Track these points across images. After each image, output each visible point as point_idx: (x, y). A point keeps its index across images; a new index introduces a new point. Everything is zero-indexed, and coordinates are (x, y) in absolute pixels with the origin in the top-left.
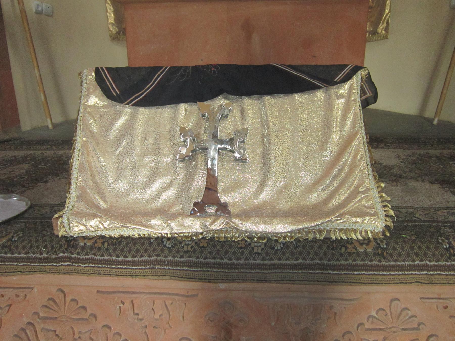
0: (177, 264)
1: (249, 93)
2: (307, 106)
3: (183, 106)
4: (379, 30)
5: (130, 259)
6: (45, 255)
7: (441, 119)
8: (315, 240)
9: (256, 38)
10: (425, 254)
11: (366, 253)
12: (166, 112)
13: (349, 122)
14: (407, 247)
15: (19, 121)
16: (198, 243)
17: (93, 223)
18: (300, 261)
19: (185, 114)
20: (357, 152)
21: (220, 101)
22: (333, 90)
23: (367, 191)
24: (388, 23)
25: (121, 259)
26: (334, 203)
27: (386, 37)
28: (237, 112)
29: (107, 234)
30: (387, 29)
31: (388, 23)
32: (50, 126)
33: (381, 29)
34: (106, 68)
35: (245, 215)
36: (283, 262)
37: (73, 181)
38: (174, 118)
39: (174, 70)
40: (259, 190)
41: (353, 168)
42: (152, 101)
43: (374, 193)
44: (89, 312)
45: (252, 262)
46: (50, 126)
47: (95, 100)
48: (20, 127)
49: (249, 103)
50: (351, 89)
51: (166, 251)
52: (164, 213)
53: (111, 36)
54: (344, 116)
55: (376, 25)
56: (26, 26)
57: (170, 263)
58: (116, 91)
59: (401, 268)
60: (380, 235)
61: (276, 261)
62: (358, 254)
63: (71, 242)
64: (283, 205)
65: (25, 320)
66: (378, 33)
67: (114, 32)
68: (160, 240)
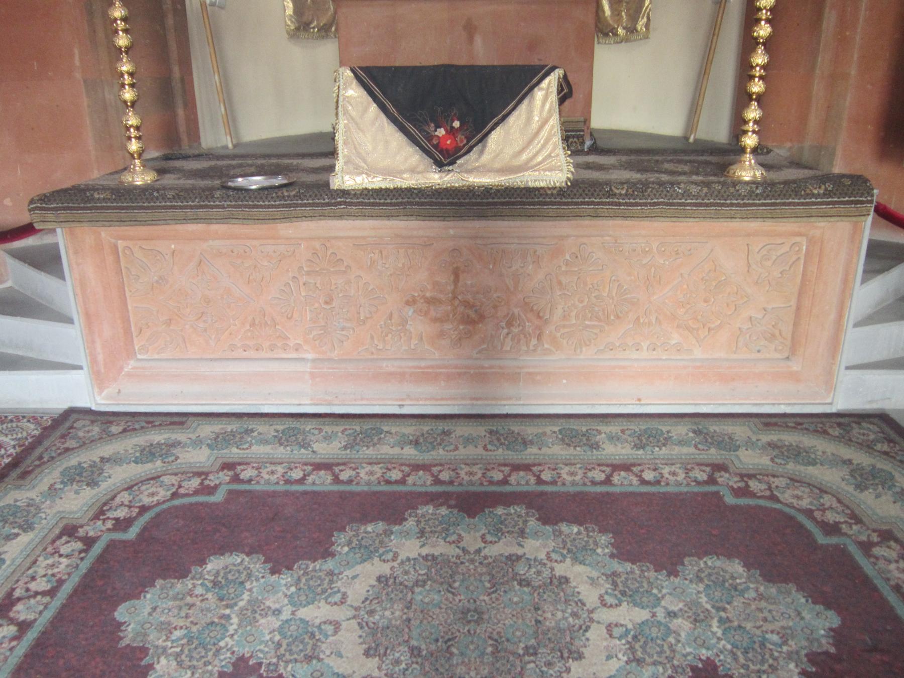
0: (423, 204)
4: (639, 28)
5: (389, 201)
6: (327, 201)
7: (697, 137)
8: (518, 188)
10: (592, 194)
11: (552, 194)
13: (547, 106)
14: (581, 191)
15: (199, 138)
16: (436, 190)
18: (507, 199)
20: (553, 126)
23: (558, 155)
24: (649, 19)
25: (382, 201)
26: (535, 162)
27: (646, 37)
29: (370, 187)
30: (647, 26)
31: (649, 19)
32: (230, 146)
33: (641, 24)
36: (496, 200)
43: (562, 157)
44: (345, 264)
45: (474, 200)
46: (230, 146)
50: (549, 83)
51: (414, 196)
53: (288, 33)
55: (634, 19)
56: (207, 23)
57: (417, 204)
59: (576, 204)
60: (563, 184)
61: (490, 200)
62: (547, 194)
63: (344, 193)
64: (497, 165)
65: (291, 274)
66: (637, 31)
67: (292, 28)
68: (409, 190)
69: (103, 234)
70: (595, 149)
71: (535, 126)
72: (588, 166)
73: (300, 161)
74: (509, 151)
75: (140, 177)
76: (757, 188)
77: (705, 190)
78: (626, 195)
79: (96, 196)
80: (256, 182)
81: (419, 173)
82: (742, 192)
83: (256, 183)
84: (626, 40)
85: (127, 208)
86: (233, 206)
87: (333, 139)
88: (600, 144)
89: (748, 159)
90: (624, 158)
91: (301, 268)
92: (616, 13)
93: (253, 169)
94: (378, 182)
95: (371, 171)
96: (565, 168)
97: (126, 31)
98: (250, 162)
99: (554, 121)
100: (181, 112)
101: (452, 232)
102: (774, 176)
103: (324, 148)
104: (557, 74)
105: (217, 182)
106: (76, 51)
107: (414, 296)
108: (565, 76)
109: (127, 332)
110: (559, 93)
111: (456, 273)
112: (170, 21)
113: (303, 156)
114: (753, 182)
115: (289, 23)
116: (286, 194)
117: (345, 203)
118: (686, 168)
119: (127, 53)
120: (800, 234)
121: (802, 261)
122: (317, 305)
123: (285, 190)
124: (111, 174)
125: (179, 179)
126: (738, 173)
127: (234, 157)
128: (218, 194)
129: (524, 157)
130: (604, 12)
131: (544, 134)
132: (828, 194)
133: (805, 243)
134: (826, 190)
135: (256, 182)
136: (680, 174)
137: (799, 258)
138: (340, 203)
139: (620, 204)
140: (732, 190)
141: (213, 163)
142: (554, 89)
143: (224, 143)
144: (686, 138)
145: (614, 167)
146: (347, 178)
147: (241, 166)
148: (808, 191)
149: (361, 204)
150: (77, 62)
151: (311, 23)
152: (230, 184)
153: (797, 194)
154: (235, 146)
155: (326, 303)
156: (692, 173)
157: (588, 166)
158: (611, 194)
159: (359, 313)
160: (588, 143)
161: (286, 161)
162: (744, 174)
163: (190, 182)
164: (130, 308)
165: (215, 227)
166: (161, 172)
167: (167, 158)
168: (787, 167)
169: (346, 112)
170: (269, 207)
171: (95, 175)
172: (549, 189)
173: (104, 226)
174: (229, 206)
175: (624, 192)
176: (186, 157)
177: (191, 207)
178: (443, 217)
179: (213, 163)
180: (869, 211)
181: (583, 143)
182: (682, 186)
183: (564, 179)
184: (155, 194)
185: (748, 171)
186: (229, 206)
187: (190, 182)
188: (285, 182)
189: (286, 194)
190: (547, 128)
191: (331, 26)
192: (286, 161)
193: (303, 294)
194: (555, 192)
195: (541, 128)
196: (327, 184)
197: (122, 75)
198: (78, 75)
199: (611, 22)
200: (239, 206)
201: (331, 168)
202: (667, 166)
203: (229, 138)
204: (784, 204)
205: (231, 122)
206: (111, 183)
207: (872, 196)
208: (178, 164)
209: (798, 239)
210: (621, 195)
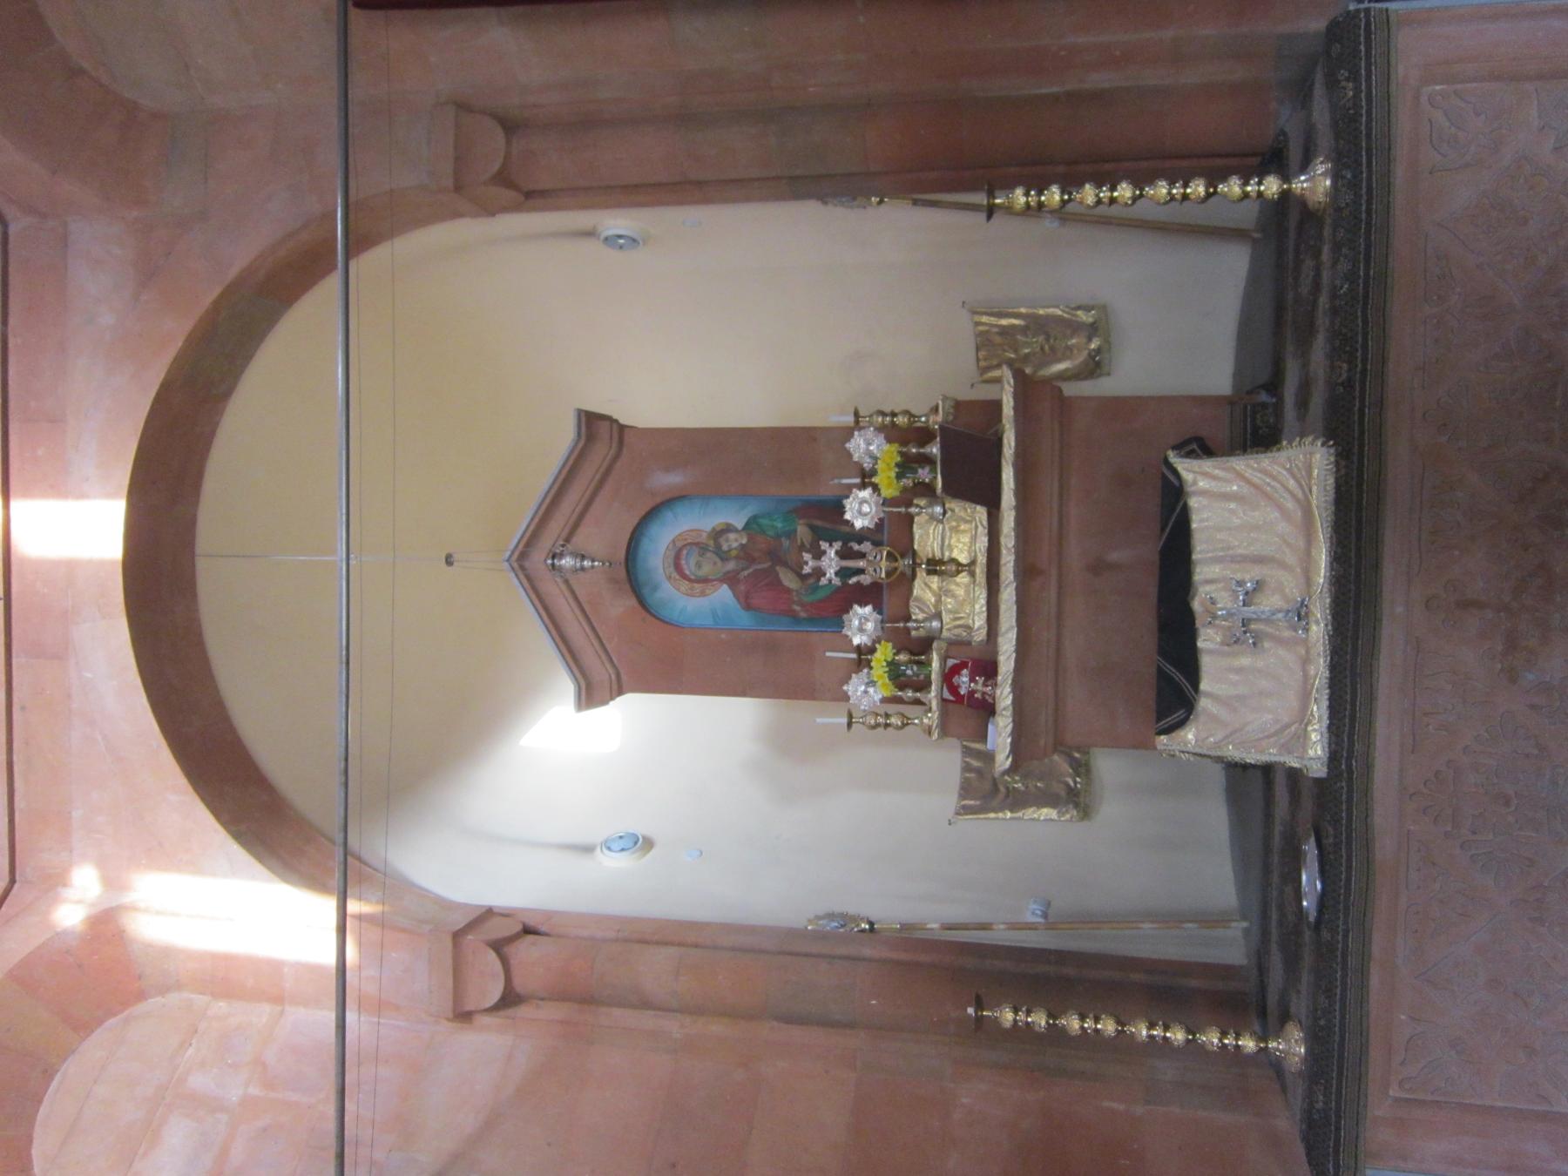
1: (1188, 574)
2: (1204, 517)
3: (1200, 644)
4: (1091, 320)
9: (1114, 556)
12: (1207, 663)
17: (1314, 737)
19: (1208, 639)
20: (1248, 466)
21: (1196, 605)
22: (1189, 489)
24: (1079, 308)
26: (1300, 495)
27: (1103, 309)
28: (1208, 588)
29: (1326, 722)
30: (1087, 309)
32: (1245, 924)
34: (1159, 720)
35: (1308, 582)
37: (1273, 759)
38: (1211, 652)
39: (1162, 652)
40: (1282, 565)
41: (1265, 472)
42: (1192, 671)
47: (1189, 735)
48: (1241, 967)
49: (1201, 573)
52: (1306, 661)
53: (1082, 819)
54: (1214, 478)
55: (1074, 327)
58: (1181, 713)
63: (1333, 758)
64: (1301, 543)
69: (1378, 1113)
70: (1274, 386)
71: (1246, 490)
72: (1303, 404)
73: (1278, 821)
74: (1283, 527)
75: (1292, 1046)
76: (1343, 177)
77: (1344, 250)
78: (1349, 362)
79: (1320, 1105)
80: (1310, 881)
81: (1307, 652)
82: (1349, 198)
83: (1311, 883)
84: (1107, 341)
85: (1340, 1068)
86: (1346, 915)
87: (1245, 767)
88: (1264, 376)
89: (1300, 184)
90: (1290, 348)
91: (1447, 834)
92: (1068, 352)
93: (1289, 889)
94: (1319, 711)
95: (1303, 718)
96: (1308, 448)
97: (1097, 1020)
98: (1275, 893)
99: (1239, 463)
100: (1194, 983)
101: (1399, 610)
102: (1325, 139)
103: (1251, 784)
104: (1173, 458)
105: (1308, 935)
106: (1106, 1104)
107: (1502, 670)
108: (1174, 448)
109: (1544, 1117)
110: (1198, 457)
111: (1466, 604)
112: (1070, 971)
113: (1268, 816)
114: (1336, 176)
115: (1068, 816)
116: (1331, 840)
117: (1349, 758)
118: (1309, 263)
119: (1123, 1025)
120: (1417, 97)
121: (1459, 86)
122: (1511, 819)
123: (1324, 841)
124: (1284, 1089)
125: (1298, 992)
126: (1321, 198)
127: (1265, 915)
128: (1326, 935)
129: (1290, 505)
130: (1066, 370)
131: (1257, 478)
132: (1354, 77)
133: (1430, 89)
134: (1348, 80)
135: (1310, 881)
136: (1318, 275)
137: (1455, 92)
138: (1349, 766)
139: (1364, 370)
140: (1346, 213)
141: (1274, 947)
142: (1195, 464)
143: (1239, 934)
144: (1255, 241)
145: (1305, 366)
146: (1311, 753)
147: (1281, 908)
148: (1350, 104)
149: (1351, 736)
150: (1122, 1107)
151: (1068, 785)
152: (1312, 919)
153: (1355, 119)
154: (1244, 918)
155: (1507, 803)
156: (1317, 254)
157: (1303, 404)
158: (1348, 384)
159: (1527, 756)
160: (1264, 397)
161: (1277, 840)
162: (1321, 189)
163: (1306, 978)
164: (1500, 1104)
165: (1376, 950)
166: (1285, 1017)
167: (1263, 1013)
168: (1309, 115)
169: (1217, 745)
170: (1349, 867)
171: (1286, 1123)
172: (1338, 471)
173: (1365, 1106)
174: (1346, 923)
175: (1345, 366)
176: (1263, 987)
177: (1344, 976)
178: (1376, 621)
179: (1274, 947)
180: (1381, 10)
181: (1264, 406)
182: (1338, 282)
183: (1324, 449)
184: (1322, 1022)
185: (1315, 183)
186: (1346, 923)
187: (1306, 978)
188: (1312, 840)
189: (1331, 840)
190: (1248, 473)
191: (1075, 759)
192: (1277, 840)
193: (1491, 836)
194: (1343, 463)
195: (1248, 482)
196: (1318, 781)
197: (1151, 1037)
198: (1139, 1110)
199: (1081, 359)
200: (1347, 908)
201: (1294, 775)
202: (1305, 290)
203: (1234, 924)
204: (1369, 135)
205: (1211, 920)
206: (1298, 1091)
207: (1358, 11)
208: (1272, 999)
209: (1424, 100)
210: (1350, 370)
